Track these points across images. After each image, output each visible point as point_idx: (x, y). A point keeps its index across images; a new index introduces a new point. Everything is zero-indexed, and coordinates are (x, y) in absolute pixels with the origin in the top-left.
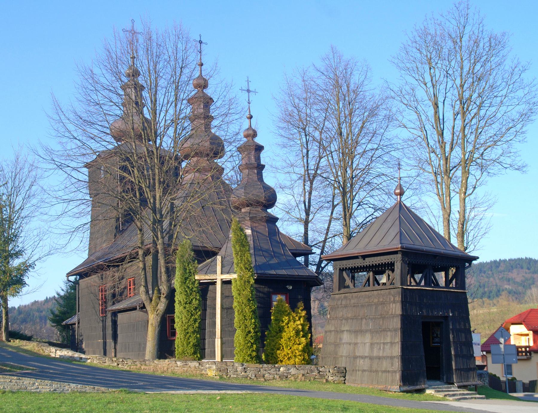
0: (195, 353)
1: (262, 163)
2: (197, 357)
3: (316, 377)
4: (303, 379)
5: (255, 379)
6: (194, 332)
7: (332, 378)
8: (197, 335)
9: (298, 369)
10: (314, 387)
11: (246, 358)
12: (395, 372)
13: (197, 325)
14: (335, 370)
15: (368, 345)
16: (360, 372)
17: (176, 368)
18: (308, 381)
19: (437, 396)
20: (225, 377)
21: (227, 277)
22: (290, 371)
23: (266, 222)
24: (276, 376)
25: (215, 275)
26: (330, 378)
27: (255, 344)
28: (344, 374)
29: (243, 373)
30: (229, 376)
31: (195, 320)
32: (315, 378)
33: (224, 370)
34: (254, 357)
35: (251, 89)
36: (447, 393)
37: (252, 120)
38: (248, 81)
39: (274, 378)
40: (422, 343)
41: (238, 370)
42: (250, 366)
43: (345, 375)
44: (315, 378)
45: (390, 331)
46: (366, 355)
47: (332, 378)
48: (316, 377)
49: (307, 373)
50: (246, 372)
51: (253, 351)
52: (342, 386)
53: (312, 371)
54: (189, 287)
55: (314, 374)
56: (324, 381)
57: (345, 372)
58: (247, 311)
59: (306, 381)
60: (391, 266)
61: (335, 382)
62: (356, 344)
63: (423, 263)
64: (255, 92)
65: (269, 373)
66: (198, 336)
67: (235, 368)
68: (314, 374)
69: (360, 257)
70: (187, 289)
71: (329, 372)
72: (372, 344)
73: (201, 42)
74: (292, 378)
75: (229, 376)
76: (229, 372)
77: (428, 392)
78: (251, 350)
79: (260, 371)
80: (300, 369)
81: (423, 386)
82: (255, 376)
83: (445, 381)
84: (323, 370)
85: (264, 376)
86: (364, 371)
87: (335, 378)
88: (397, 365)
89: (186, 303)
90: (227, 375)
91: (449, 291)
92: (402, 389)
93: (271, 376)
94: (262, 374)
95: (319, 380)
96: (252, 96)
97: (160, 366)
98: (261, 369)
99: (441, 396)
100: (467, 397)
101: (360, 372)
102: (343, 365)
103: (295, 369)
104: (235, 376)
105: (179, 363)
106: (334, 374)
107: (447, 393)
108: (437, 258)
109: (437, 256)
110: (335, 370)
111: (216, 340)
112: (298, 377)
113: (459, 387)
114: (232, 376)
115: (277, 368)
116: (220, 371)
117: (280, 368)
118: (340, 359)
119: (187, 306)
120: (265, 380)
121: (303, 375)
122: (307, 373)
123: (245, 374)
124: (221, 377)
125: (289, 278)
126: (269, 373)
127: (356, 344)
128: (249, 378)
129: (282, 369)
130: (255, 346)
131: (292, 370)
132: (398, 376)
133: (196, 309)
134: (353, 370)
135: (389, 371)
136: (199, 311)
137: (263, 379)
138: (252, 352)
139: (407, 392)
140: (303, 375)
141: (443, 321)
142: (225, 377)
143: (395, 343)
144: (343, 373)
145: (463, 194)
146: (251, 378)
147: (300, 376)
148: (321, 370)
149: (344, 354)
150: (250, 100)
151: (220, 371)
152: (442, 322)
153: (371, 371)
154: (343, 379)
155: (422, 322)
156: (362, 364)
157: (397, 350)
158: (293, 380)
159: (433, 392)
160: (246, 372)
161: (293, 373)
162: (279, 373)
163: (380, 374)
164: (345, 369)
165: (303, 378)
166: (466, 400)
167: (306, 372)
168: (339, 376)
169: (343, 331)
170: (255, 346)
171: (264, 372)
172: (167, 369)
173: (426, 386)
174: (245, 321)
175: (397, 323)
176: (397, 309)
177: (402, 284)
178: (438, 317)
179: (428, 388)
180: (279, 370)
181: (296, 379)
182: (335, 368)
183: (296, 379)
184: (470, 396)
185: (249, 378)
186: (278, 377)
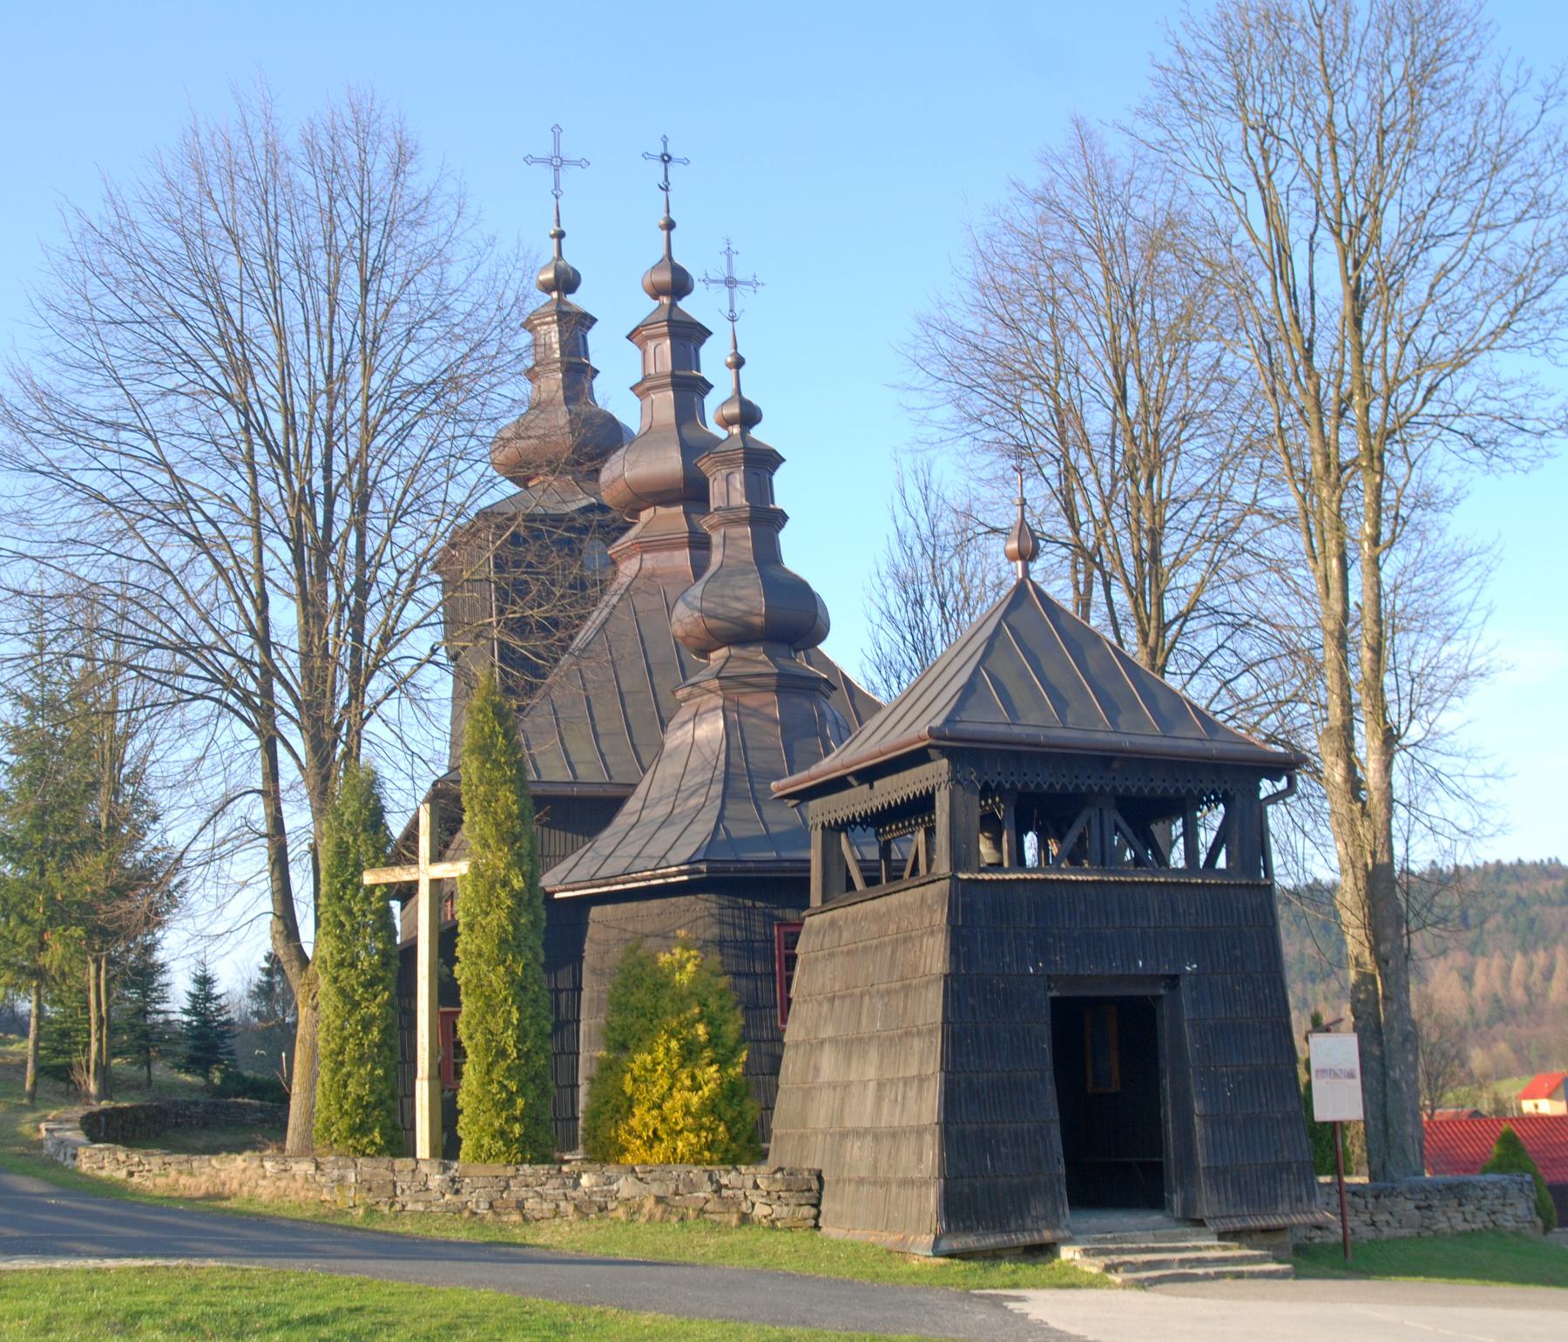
0: (360, 1129)
1: (780, 502)
2: (372, 1143)
3: (709, 1207)
4: (658, 1216)
5: (490, 1215)
6: (361, 1061)
7: (767, 1210)
8: (373, 1069)
9: (641, 1180)
10: (705, 1245)
11: (486, 1141)
12: (925, 1183)
13: (375, 1034)
14: (775, 1181)
15: (872, 1086)
16: (853, 1186)
17: (261, 1182)
18: (674, 1219)
19: (1086, 1269)
20: (386, 1209)
21: (444, 870)
22: (615, 1187)
23: (777, 692)
24: (563, 1204)
25: (413, 869)
26: (761, 1210)
27: (524, 1095)
28: (815, 1193)
29: (448, 1196)
30: (398, 1207)
31: (366, 1024)
32: (702, 1211)
33: (382, 1187)
34: (517, 1140)
35: (738, 276)
36: (1116, 1259)
37: (742, 371)
38: (729, 253)
39: (557, 1213)
40: (1049, 1075)
41: (431, 1184)
42: (472, 1172)
43: (819, 1199)
44: (702, 1211)
45: (919, 1033)
46: (866, 1123)
47: (767, 1210)
48: (709, 1207)
49: (676, 1193)
50: (457, 1192)
51: (512, 1119)
52: (802, 1239)
53: (693, 1186)
54: (349, 912)
55: (701, 1195)
56: (734, 1221)
57: (815, 1185)
58: (497, 978)
59: (668, 1221)
60: (921, 806)
61: (779, 1224)
62: (847, 1086)
63: (1177, 790)
64: (754, 284)
65: (540, 1195)
66: (380, 1072)
67: (421, 1177)
68: (701, 1195)
69: (851, 780)
70: (343, 918)
71: (756, 1186)
72: (881, 1085)
73: (666, 159)
74: (621, 1213)
75: (398, 1207)
76: (399, 1192)
77: (1068, 1253)
78: (504, 1114)
79: (507, 1187)
80: (649, 1177)
81: (1047, 1235)
82: (491, 1206)
83: (1178, 1213)
84: (734, 1183)
85: (520, 1205)
86: (861, 1181)
87: (780, 1210)
88: (926, 1158)
89: (340, 964)
90: (392, 1205)
91: (1064, 881)
92: (945, 1245)
93: (545, 1206)
94: (513, 1199)
95: (717, 1217)
96: (743, 297)
97: (223, 1175)
98: (512, 1182)
99: (1095, 1270)
100: (1200, 1271)
101: (853, 1186)
102: (817, 1166)
103: (631, 1179)
104: (420, 1207)
105: (268, 1165)
106: (774, 1195)
107: (1116, 1259)
108: (1116, 765)
109: (1113, 759)
110: (775, 1181)
111: (418, 1083)
112: (641, 1206)
113: (1222, 1236)
114: (410, 1207)
115: (568, 1176)
116: (370, 1190)
117: (579, 1176)
118: (813, 1139)
119: (343, 973)
120: (525, 1219)
121: (659, 1200)
122: (676, 1193)
123: (455, 1199)
124: (371, 1211)
125: (757, 871)
126: (540, 1195)
127: (847, 1086)
128: (466, 1214)
129: (585, 1180)
130: (520, 1102)
131: (622, 1181)
132: (931, 1198)
133: (369, 984)
134: (838, 1181)
135: (913, 1182)
136: (385, 989)
137: (516, 1217)
138: (507, 1121)
139: (965, 1255)
140: (659, 1200)
141: (1162, 992)
142: (386, 1209)
143: (928, 1078)
144: (810, 1190)
145: (1366, 545)
146: (474, 1214)
147: (649, 1204)
148: (724, 1181)
149: (821, 1126)
150: (737, 311)
151: (370, 1190)
152: (1160, 997)
153: (875, 1183)
154: (808, 1211)
155: (1053, 999)
156: (858, 1154)
157: (927, 1106)
158: (623, 1218)
159: (1077, 1256)
160: (457, 1192)
161: (624, 1194)
162: (574, 1194)
163: (894, 1189)
164: (820, 1178)
165: (658, 1211)
166: (1186, 1286)
167: (672, 1187)
168: (793, 1201)
169: (822, 1043)
170: (520, 1102)
171: (523, 1193)
172: (241, 1185)
173: (1060, 1234)
174: (489, 1017)
175: (930, 1007)
176: (934, 955)
177: (956, 865)
178: (1139, 979)
179: (1069, 1241)
180: (577, 1184)
181: (633, 1214)
182: (779, 1175)
183: (633, 1214)
184: (1211, 1270)
185: (466, 1214)
186: (571, 1209)
